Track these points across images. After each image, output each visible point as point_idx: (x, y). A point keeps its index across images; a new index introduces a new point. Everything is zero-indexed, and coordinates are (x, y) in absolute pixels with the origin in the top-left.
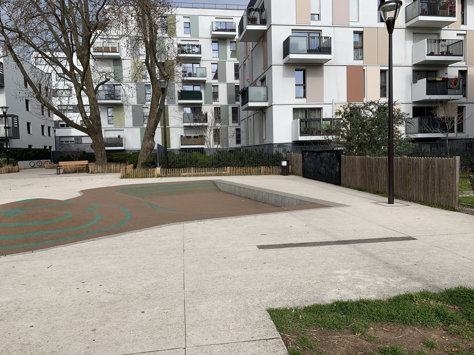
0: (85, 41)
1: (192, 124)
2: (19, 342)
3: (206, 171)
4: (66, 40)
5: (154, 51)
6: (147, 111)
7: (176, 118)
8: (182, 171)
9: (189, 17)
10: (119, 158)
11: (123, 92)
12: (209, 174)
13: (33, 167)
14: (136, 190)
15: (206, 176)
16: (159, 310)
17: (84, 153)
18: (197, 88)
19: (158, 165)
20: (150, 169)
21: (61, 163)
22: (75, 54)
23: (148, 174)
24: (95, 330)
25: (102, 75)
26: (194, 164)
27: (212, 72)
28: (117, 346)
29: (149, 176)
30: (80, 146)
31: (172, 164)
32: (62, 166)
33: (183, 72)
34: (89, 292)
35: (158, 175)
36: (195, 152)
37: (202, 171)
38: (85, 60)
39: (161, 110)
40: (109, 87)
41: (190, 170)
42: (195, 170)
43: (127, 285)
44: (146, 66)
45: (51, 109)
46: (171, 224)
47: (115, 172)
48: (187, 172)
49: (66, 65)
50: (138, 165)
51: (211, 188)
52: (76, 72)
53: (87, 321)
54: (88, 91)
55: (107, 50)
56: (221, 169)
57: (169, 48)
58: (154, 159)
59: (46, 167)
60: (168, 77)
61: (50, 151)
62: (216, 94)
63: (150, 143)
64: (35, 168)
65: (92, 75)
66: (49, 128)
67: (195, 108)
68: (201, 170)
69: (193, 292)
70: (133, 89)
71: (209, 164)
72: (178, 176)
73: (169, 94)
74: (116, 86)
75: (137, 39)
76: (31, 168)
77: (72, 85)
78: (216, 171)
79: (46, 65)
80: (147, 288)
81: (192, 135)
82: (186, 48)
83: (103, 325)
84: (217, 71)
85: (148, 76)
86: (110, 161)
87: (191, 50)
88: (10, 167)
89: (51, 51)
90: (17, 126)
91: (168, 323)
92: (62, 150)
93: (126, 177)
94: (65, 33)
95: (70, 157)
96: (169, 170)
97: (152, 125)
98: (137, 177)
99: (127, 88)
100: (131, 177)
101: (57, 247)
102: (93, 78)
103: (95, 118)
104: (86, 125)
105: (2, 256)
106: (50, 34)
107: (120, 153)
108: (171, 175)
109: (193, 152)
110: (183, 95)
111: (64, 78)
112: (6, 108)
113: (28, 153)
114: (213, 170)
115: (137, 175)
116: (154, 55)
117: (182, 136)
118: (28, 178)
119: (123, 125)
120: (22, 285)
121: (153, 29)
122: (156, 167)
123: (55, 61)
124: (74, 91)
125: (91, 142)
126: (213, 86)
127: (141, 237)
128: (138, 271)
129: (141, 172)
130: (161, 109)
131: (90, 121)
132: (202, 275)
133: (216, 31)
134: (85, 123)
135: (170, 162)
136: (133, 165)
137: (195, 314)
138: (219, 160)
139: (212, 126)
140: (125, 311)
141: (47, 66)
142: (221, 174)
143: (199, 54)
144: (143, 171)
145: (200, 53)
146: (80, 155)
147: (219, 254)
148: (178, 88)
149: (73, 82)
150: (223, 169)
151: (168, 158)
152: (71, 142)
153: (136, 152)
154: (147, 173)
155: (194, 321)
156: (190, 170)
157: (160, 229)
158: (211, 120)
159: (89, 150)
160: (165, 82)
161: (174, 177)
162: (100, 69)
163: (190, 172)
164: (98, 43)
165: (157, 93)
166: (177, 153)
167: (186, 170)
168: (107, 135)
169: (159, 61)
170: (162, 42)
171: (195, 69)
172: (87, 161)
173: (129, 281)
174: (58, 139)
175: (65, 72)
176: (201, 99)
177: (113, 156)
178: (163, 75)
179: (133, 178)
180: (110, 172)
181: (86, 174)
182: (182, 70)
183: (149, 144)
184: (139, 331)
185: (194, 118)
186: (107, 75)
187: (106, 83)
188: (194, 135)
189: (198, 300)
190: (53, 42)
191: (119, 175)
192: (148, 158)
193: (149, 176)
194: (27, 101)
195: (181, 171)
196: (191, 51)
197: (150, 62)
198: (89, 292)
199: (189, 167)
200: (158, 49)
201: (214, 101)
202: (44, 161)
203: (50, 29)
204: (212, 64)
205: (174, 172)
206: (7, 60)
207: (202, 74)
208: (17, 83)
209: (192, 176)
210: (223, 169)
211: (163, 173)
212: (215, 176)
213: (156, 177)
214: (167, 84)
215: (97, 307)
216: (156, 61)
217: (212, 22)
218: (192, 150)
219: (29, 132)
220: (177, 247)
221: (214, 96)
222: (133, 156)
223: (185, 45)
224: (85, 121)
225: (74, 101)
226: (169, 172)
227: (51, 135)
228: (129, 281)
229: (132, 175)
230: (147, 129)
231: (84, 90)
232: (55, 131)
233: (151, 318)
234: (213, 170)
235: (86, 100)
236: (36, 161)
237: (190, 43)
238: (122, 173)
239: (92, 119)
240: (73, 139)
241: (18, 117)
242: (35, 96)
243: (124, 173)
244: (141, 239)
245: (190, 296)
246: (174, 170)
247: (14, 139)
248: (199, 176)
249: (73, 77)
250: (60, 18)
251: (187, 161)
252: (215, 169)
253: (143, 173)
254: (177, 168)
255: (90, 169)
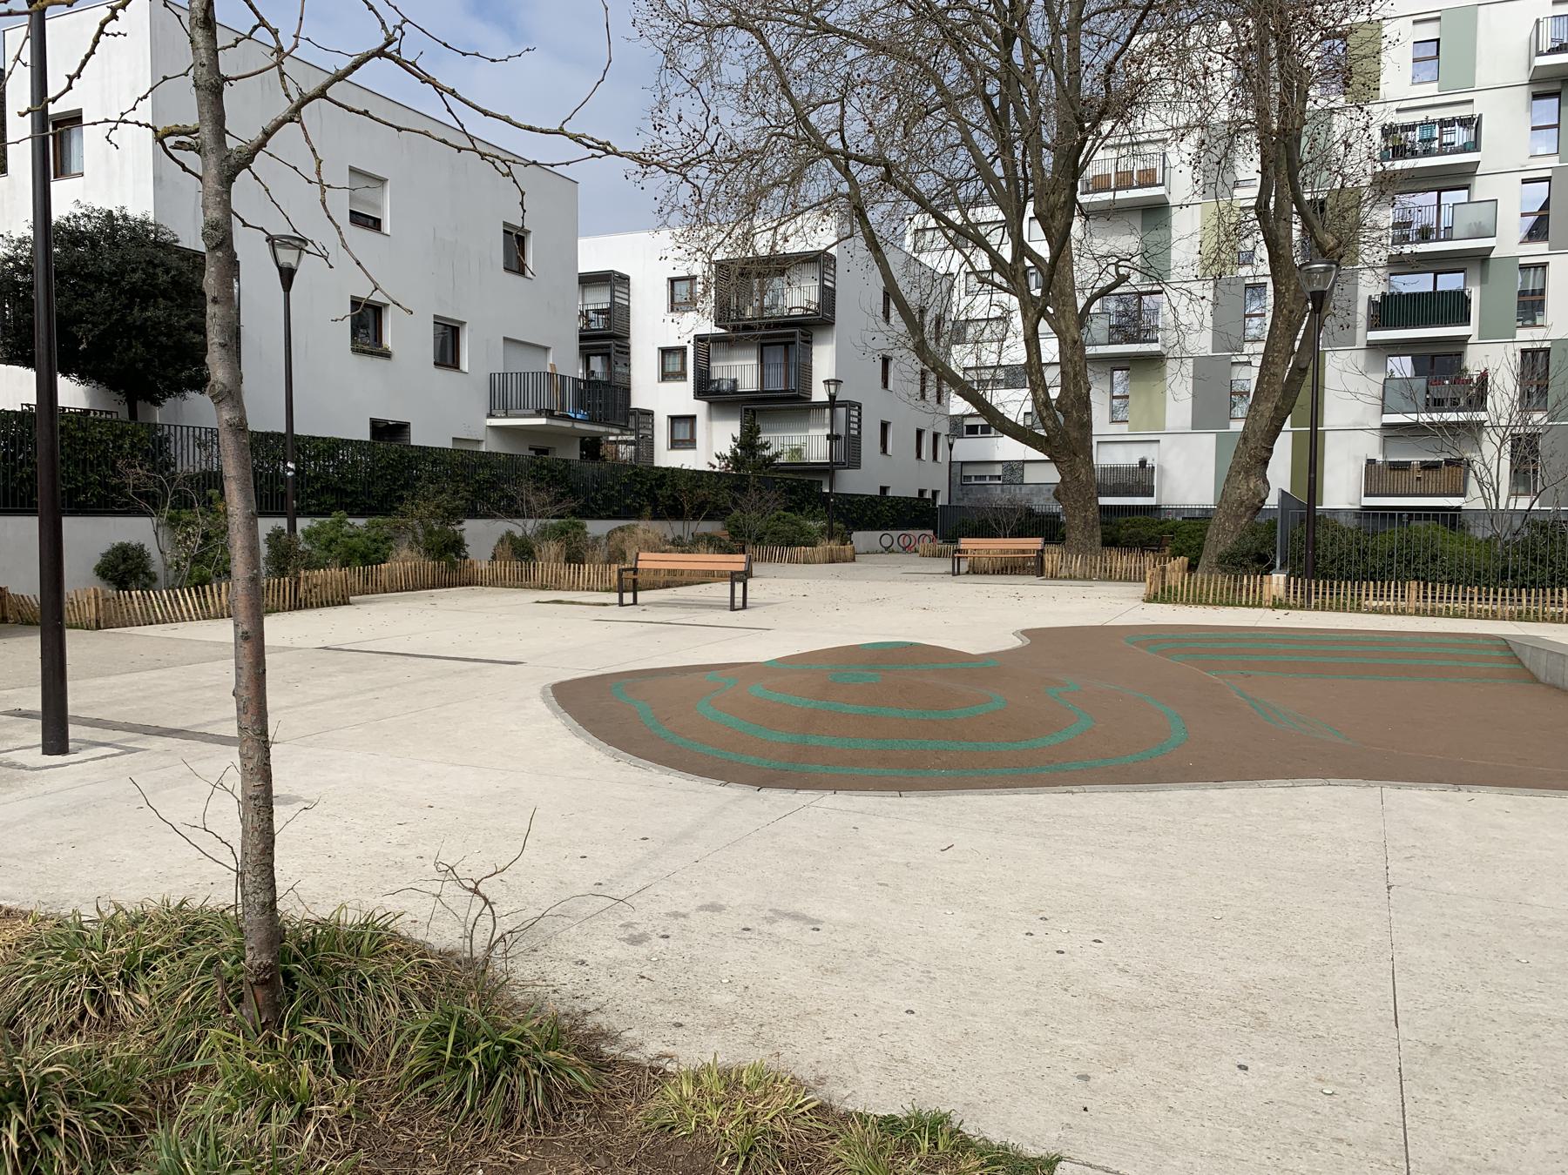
0: (1062, 162)
1: (1424, 418)
2: (880, 1047)
3: (1472, 599)
4: (1009, 167)
5: (1294, 165)
6: (1248, 377)
7: (1358, 396)
8: (1371, 593)
9: (1438, 19)
10: (1139, 533)
11: (1170, 317)
12: (1486, 610)
13: (888, 550)
14: (1199, 645)
15: (1471, 617)
16: (1302, 1078)
17: (1030, 512)
18: (1450, 282)
19: (1278, 565)
20: (1249, 579)
21: (966, 543)
22: (1030, 206)
23: (1241, 596)
24: (1085, 1078)
25: (1104, 266)
26: (1421, 566)
27: (1523, 215)
28: (1159, 1153)
29: (1244, 599)
30: (1018, 491)
31: (1333, 562)
32: (966, 551)
33: (1395, 226)
34: (1063, 952)
35: (1274, 599)
36: (1422, 524)
37: (1456, 598)
38: (1058, 223)
39: (1301, 369)
40: (1121, 301)
41: (1403, 592)
42: (1425, 593)
43: (1184, 961)
44: (1257, 223)
45: (949, 379)
46: (1332, 781)
47: (1126, 578)
48: (1389, 596)
49: (1001, 243)
50: (1204, 562)
51: (1490, 665)
52: (1028, 263)
53: (1062, 1041)
54: (1058, 319)
55: (1125, 181)
56: (1544, 595)
57: (1348, 145)
58: (1264, 544)
59: (921, 551)
60: (1341, 250)
61: (934, 504)
62: (1533, 298)
63: (1252, 486)
64: (893, 552)
65: (1075, 268)
66: (936, 436)
67: (1433, 357)
68: (1449, 591)
69: (1435, 1048)
70: (1204, 303)
71: (1486, 571)
72: (1352, 610)
73: (1336, 312)
74: (1146, 298)
75: (1235, 130)
76: (882, 552)
77: (1014, 302)
78: (1519, 600)
79: (945, 249)
80: (1255, 987)
81: (1415, 459)
82: (1416, 136)
83: (1110, 1070)
84: (1546, 206)
85: (1262, 252)
86: (1111, 542)
87: (1437, 142)
88: (834, 545)
89: (964, 207)
90: (856, 433)
91: (1341, 1134)
92: (965, 503)
93: (1162, 597)
94: (1006, 146)
95: (990, 526)
96: (1317, 586)
97: (1263, 422)
98: (1200, 603)
99: (1185, 300)
100: (1181, 600)
101: (963, 794)
102: (1079, 278)
103: (1073, 405)
104: (1045, 427)
105: (828, 793)
106: (963, 158)
107: (1142, 518)
108: (1324, 603)
109: (1414, 523)
110: (1388, 311)
111: (993, 284)
112: (837, 382)
113: (879, 508)
114: (1504, 594)
115: (1201, 593)
116: (1292, 176)
117: (1371, 462)
118: (877, 580)
119: (1157, 423)
120: (881, 884)
121: (1295, 84)
122: (1269, 569)
123: (967, 236)
124: (1017, 321)
125: (1057, 478)
126: (1524, 267)
127: (1225, 810)
128: (1221, 923)
129: (1216, 583)
130: (1303, 366)
131: (1058, 413)
132: (1470, 995)
133: (1552, 51)
134: (1042, 420)
135: (1324, 556)
136: (1186, 559)
137: (1445, 1132)
138: (1534, 560)
139: (1513, 423)
140: (1182, 1045)
141: (949, 253)
142: (1540, 615)
143: (1469, 151)
144: (1223, 582)
145: (1474, 146)
146: (1019, 519)
147: (1542, 931)
148: (1369, 286)
149: (1019, 293)
150: (1553, 594)
151: (1315, 541)
152: (992, 477)
153: (1197, 514)
154: (1235, 590)
155: (1443, 1156)
156: (1403, 592)
157: (1289, 791)
158: (1508, 402)
159: (1046, 504)
160: (1328, 270)
161: (1337, 610)
162: (1101, 245)
163: (1403, 597)
164: (1102, 162)
165: (1291, 312)
166: (1351, 523)
167: (1386, 589)
168: (1106, 457)
169: (1307, 197)
170: (1325, 127)
171: (1446, 214)
172: (1040, 540)
173: (1190, 951)
174: (956, 469)
175: (998, 266)
176: (1466, 320)
177: (1120, 526)
178: (1319, 245)
179: (1186, 604)
180: (1110, 579)
181: (1034, 579)
182: (1391, 221)
183: (1249, 489)
184: (1233, 1129)
185: (1428, 392)
186: (1120, 263)
187: (1117, 290)
188: (1423, 459)
189: (1456, 1084)
190: (969, 180)
191: (1141, 589)
192: (1243, 538)
193: (1244, 599)
194: (886, 361)
195: (1364, 593)
196: (1436, 144)
197: (1272, 206)
198: (1063, 952)
199: (1397, 578)
200: (1306, 157)
201: (1524, 326)
202: (916, 533)
203: (967, 140)
204: (1524, 181)
205: (1338, 594)
206: (850, 248)
207: (1479, 225)
208: (870, 312)
209: (1411, 614)
210: (1553, 594)
211: (1295, 593)
212: (1512, 619)
213: (1268, 607)
214: (1335, 278)
215: (1091, 1008)
216: (1297, 199)
217: (1538, 21)
218: (1410, 515)
219: (884, 451)
220: (1361, 868)
221: (1522, 305)
222: (1188, 528)
223: (1412, 127)
224: (1044, 415)
225: (1017, 354)
226: (1317, 593)
227: (940, 459)
228: (1190, 951)
229: (1182, 594)
230: (1244, 437)
231: (1048, 317)
232: (951, 446)
233: (1272, 1095)
234: (1504, 594)
235: (1050, 348)
236: (895, 533)
237: (1435, 115)
238: (1151, 584)
239: (1063, 409)
240: (998, 470)
241: (860, 408)
242: (910, 344)
243: (1156, 587)
244: (1224, 815)
245: (1421, 1061)
246: (1339, 586)
247: (848, 468)
248: (1440, 616)
249: (1020, 279)
250: (996, 102)
251: (1391, 556)
252: (1511, 594)
253: (1222, 589)
254: (1348, 578)
255: (1048, 565)
